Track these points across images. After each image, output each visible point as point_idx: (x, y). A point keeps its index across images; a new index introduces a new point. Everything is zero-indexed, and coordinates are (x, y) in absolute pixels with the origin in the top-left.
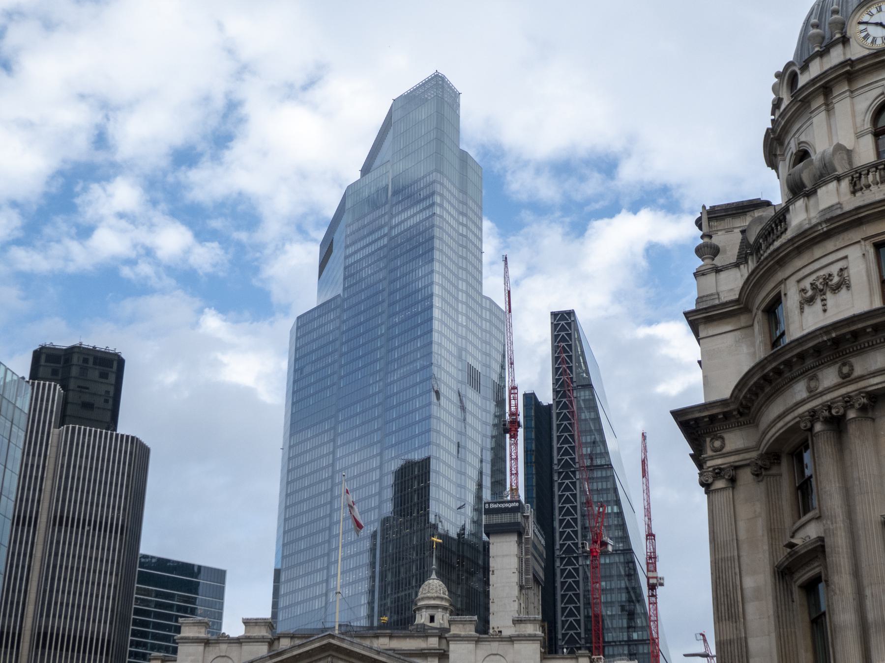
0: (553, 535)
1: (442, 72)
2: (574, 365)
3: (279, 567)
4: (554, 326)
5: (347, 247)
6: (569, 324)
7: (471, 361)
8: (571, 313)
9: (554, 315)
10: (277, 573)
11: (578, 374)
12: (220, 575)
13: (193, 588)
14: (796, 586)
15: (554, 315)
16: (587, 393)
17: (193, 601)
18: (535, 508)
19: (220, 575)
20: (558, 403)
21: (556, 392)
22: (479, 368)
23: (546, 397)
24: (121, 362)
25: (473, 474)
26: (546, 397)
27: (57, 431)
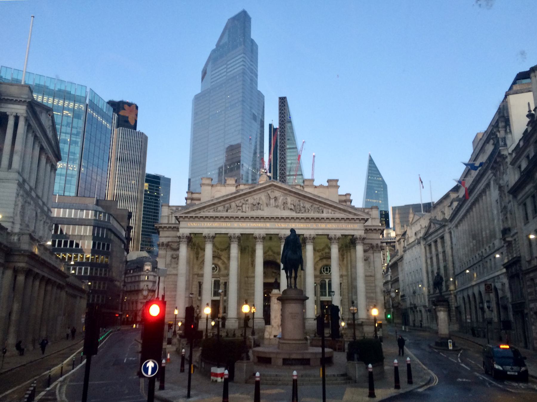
0: (8, 327)
1: (246, 10)
2: (286, 115)
3: (190, 178)
4: (280, 102)
5: (212, 71)
6: (285, 101)
7: (254, 111)
8: (285, 98)
9: (280, 98)
10: (189, 180)
11: (287, 118)
12: (169, 180)
13: (159, 183)
14: (459, 194)
15: (280, 98)
16: (290, 124)
17: (158, 187)
18: (44, 397)
19: (169, 180)
20: (280, 127)
21: (280, 124)
22: (256, 114)
23: (276, 125)
24: (137, 108)
25: (254, 136)
26: (276, 125)
27: (116, 129)
